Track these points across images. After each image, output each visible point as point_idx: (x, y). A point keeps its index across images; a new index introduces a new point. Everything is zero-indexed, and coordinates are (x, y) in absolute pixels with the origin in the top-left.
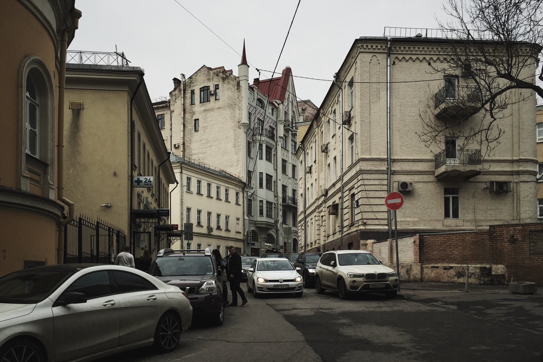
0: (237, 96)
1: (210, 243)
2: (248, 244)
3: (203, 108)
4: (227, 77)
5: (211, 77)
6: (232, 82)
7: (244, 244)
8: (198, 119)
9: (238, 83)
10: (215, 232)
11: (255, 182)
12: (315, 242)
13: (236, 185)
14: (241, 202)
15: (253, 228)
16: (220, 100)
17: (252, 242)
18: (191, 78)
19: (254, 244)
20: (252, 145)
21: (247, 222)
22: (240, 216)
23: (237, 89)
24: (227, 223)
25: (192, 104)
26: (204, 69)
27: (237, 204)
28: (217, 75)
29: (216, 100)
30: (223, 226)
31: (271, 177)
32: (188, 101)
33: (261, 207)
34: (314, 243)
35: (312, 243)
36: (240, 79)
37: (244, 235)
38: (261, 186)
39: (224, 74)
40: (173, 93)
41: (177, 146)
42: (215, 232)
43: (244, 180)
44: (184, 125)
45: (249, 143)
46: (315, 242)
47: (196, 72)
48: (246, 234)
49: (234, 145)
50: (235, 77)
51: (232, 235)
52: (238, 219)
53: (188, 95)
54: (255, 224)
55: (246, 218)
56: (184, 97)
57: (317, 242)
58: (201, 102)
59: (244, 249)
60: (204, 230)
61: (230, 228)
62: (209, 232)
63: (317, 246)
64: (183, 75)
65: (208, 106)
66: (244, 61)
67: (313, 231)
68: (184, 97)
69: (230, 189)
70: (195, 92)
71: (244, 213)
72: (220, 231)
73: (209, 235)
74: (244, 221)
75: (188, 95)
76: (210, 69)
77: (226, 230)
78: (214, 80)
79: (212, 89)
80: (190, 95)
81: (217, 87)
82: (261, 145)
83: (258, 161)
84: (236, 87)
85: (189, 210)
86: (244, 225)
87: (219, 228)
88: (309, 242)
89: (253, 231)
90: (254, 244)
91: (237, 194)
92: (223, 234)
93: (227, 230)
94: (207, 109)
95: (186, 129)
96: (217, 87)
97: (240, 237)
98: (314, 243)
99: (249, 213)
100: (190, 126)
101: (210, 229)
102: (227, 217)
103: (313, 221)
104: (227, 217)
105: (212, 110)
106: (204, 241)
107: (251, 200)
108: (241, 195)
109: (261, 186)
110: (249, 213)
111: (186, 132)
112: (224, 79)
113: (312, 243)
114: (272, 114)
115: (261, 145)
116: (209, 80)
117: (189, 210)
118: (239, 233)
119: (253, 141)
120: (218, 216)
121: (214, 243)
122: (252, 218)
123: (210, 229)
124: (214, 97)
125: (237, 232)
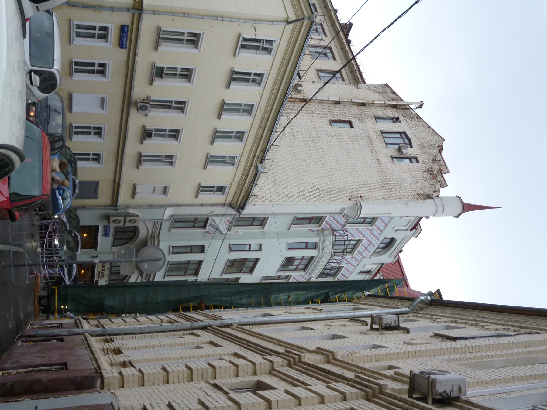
0: (407, 194)
1: (107, 102)
2: (107, 217)
3: (373, 136)
4: (435, 177)
5: (429, 151)
6: (427, 185)
7: (106, 206)
8: (352, 126)
9: (428, 197)
10: (136, 120)
11: (243, 235)
12: (124, 365)
13: (241, 184)
14: (205, 198)
15: (143, 233)
16: (393, 165)
17: (112, 226)
18: (419, 118)
19: (106, 234)
20: (315, 227)
21: (157, 214)
22: (173, 197)
23: (418, 195)
24: (156, 159)
25: (376, 118)
26: (438, 139)
27: (203, 189)
28: (434, 161)
29: (393, 158)
30: (154, 146)
31: (251, 271)
32: (380, 112)
33: (191, 249)
34: (120, 358)
35: (118, 352)
36: (436, 199)
37: (128, 207)
38: (232, 249)
39: (437, 173)
40: (387, 90)
41: (299, 88)
42: (136, 120)
43: (250, 210)
44: (338, 103)
45: (317, 220)
46: (124, 365)
47: (429, 127)
48: (131, 211)
49: (317, 188)
50: (438, 192)
51: (129, 174)
52: (165, 190)
53: (391, 113)
54: (152, 237)
55: (169, 212)
56: (385, 106)
57: (128, 372)
58: (382, 132)
59: (94, 207)
60: (141, 89)
61: (145, 166)
62: (136, 104)
63: (109, 372)
64: (421, 106)
65: (379, 143)
66: (468, 208)
67: (176, 353)
68: (385, 106)
69: (233, 168)
70: (397, 124)
71: (178, 206)
72: (138, 138)
73: (129, 103)
74: (160, 206)
75: (391, 113)
76: (441, 150)
77: (140, 155)
78: (425, 156)
79: (408, 151)
80: (391, 116)
81: (413, 159)
82: (315, 246)
83: (283, 242)
84: (421, 192)
85: (194, 40)
86: (151, 206)
87: (147, 134)
88: (119, 342)
89: (135, 231)
90: (106, 234)
91: (221, 189)
92: (132, 147)
93: (140, 159)
94: (374, 143)
95: (333, 107)
96: (413, 159)
97: (124, 198)
98: (120, 358)
99: (179, 222)
100: (338, 113)
101: (145, 105)
102: (170, 160)
103: (209, 350)
104: (170, 160)
105: (373, 150)
106: (111, 85)
107: (204, 227)
108: (218, 198)
109: (232, 249)
110: (179, 222)
111: (326, 106)
112: (430, 171)
113: (118, 352)
114: (361, 272)
115: (315, 246)
116: (423, 147)
117: (194, 40)
118: (134, 194)
119: (323, 230)
120: (175, 134)
121: (109, 121)
122: (166, 225)
123: (145, 105)
124: (396, 154)
125: (135, 187)
